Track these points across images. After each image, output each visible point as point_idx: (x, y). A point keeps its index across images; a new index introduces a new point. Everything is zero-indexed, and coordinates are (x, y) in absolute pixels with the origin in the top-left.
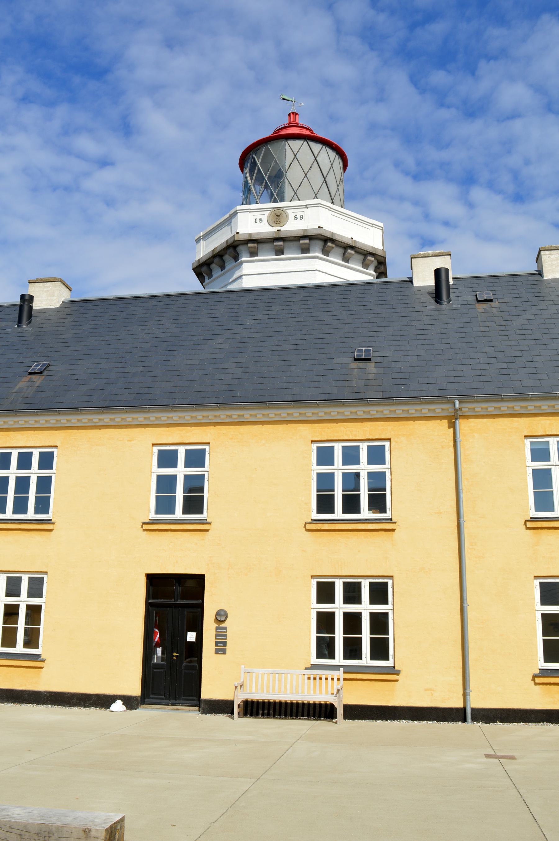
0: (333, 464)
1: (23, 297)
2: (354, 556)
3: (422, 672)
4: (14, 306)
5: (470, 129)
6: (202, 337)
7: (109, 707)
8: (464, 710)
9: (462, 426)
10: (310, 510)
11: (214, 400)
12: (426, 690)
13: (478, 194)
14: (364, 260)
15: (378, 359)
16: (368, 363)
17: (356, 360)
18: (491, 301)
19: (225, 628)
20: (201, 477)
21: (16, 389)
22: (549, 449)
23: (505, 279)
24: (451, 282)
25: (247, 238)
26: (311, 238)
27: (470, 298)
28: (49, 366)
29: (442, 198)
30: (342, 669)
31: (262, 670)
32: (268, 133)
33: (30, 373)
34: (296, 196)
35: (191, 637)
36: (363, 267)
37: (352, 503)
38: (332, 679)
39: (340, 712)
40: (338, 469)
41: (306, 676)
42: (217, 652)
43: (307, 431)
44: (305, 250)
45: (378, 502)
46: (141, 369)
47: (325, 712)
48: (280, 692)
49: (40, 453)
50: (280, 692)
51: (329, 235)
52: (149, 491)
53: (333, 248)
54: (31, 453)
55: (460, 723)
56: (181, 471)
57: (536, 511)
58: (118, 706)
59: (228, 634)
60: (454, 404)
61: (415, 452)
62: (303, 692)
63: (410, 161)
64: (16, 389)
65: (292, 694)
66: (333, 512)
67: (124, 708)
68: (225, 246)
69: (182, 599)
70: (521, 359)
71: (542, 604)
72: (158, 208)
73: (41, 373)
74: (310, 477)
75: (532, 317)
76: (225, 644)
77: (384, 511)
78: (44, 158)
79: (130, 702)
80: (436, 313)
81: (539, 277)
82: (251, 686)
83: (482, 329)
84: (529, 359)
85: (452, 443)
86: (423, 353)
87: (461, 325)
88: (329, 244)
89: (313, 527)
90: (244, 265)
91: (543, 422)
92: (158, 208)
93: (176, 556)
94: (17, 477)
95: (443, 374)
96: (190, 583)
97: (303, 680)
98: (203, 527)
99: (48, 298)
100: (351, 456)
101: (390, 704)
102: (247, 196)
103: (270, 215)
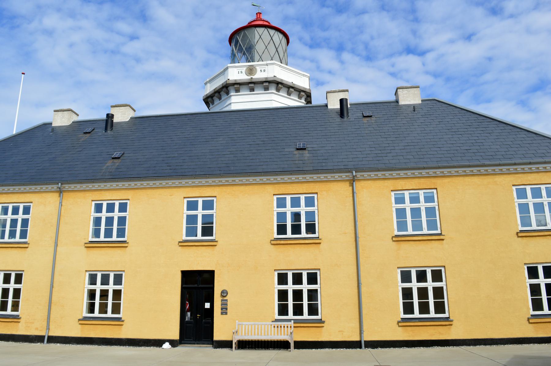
0: (286, 207)
1: (108, 115)
2: (298, 258)
3: (336, 322)
4: (103, 120)
5: (340, 19)
6: (210, 137)
7: (161, 346)
8: (360, 342)
9: (357, 185)
10: (273, 233)
11: (218, 172)
12: (339, 331)
13: (346, 56)
14: (299, 95)
15: (310, 149)
16: (304, 152)
17: (298, 149)
18: (371, 116)
19: (227, 300)
20: (212, 216)
21: (105, 167)
22: (404, 197)
23: (378, 105)
24: (349, 106)
25: (234, 82)
26: (270, 82)
27: (359, 115)
28: (123, 154)
29: (326, 58)
30: (292, 321)
31: (248, 323)
32: (245, 24)
33: (113, 158)
34: (261, 59)
35: (207, 305)
36: (299, 98)
37: (296, 229)
38: (287, 327)
39: (292, 345)
40: (289, 210)
41: (273, 326)
42: (222, 313)
43: (390, 184)
44: (266, 89)
45: (311, 228)
46: (176, 155)
47: (283, 345)
48: (258, 335)
49: (120, 203)
50: (258, 335)
51: (279, 81)
52: (182, 224)
53: (282, 88)
54: (198, 201)
55: (358, 349)
56: (200, 212)
57: (278, 234)
58: (167, 345)
59: (228, 303)
60: (352, 173)
61: (330, 201)
62: (271, 335)
63: (307, 37)
64: (105, 167)
65: (265, 335)
66: (286, 234)
67: (170, 346)
68: (221, 86)
69: (202, 284)
70: (388, 148)
71: (402, 282)
72: (166, 64)
73: (119, 158)
74: (273, 215)
75: (394, 125)
76: (226, 309)
77: (314, 232)
78: (99, 35)
79: (173, 343)
80: (341, 123)
81: (396, 104)
82: (242, 332)
83: (366, 132)
84: (393, 148)
85: (351, 195)
86: (334, 145)
87: (355, 130)
88: (280, 86)
89: (275, 242)
90: (232, 97)
91: (401, 182)
92: (166, 64)
93: (198, 261)
94: (22, 219)
95: (346, 157)
96: (206, 276)
97: (271, 328)
98: (213, 244)
99: (121, 116)
100: (296, 202)
101: (319, 340)
102: (233, 59)
103: (246, 70)
